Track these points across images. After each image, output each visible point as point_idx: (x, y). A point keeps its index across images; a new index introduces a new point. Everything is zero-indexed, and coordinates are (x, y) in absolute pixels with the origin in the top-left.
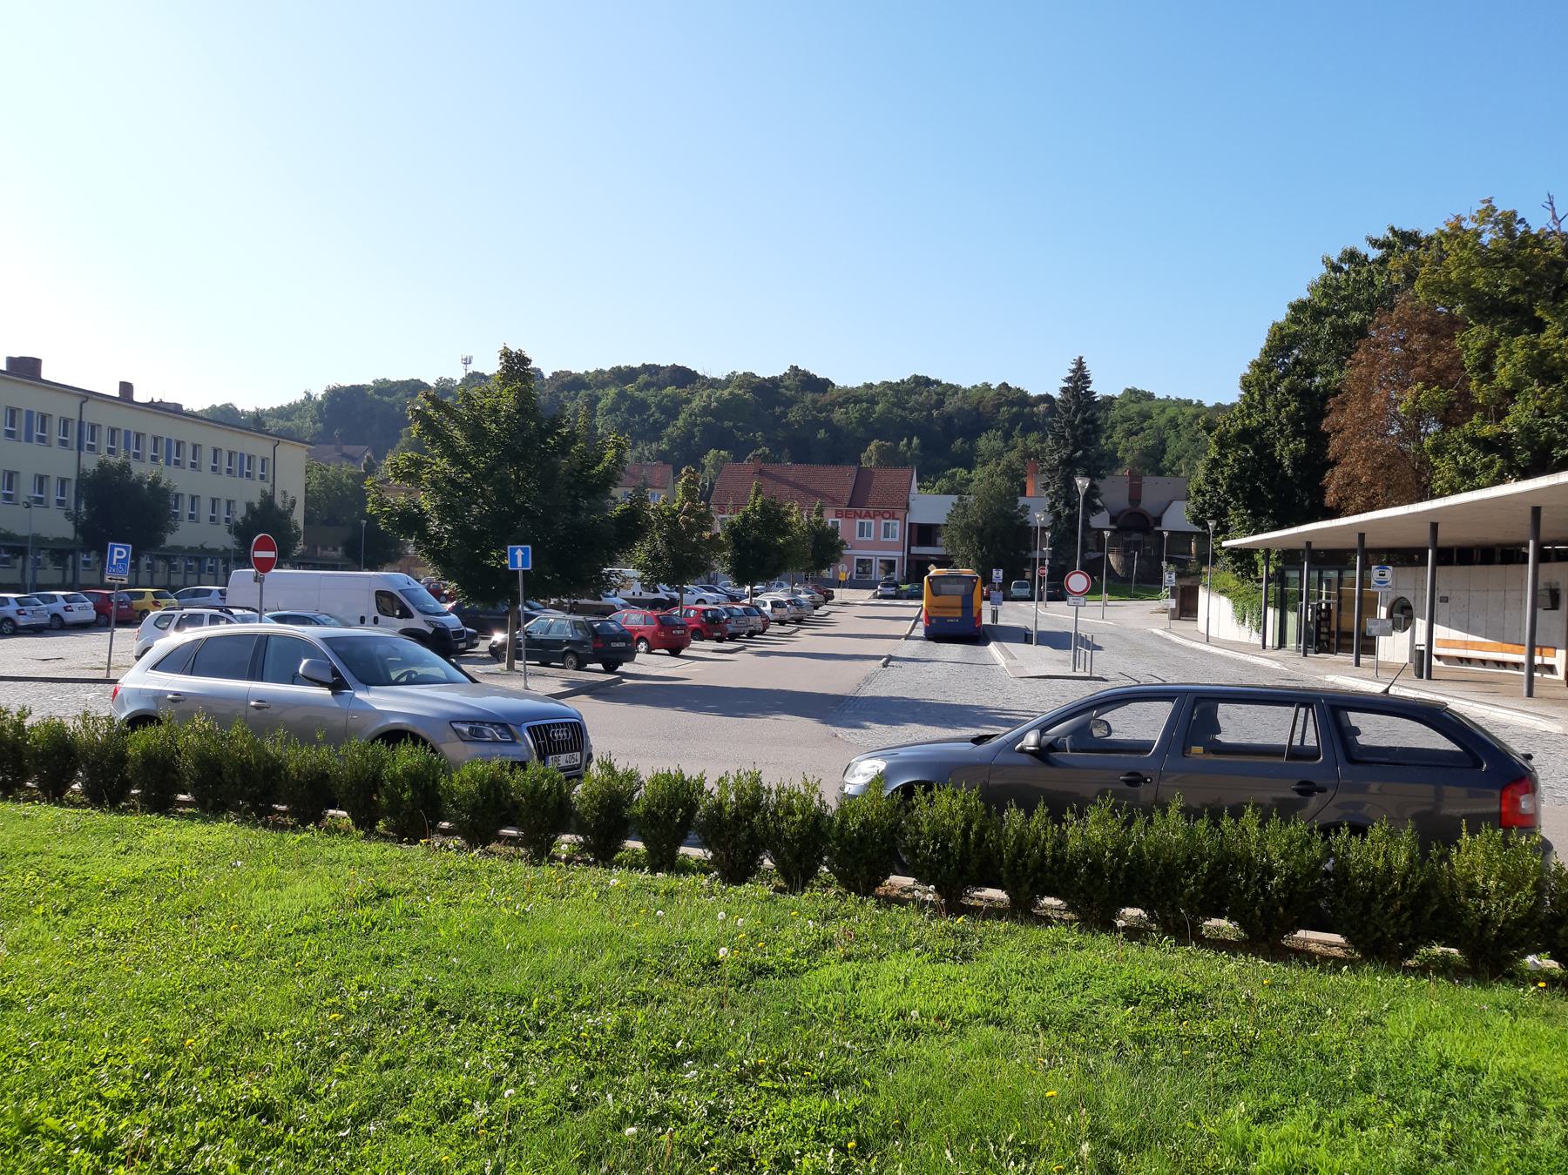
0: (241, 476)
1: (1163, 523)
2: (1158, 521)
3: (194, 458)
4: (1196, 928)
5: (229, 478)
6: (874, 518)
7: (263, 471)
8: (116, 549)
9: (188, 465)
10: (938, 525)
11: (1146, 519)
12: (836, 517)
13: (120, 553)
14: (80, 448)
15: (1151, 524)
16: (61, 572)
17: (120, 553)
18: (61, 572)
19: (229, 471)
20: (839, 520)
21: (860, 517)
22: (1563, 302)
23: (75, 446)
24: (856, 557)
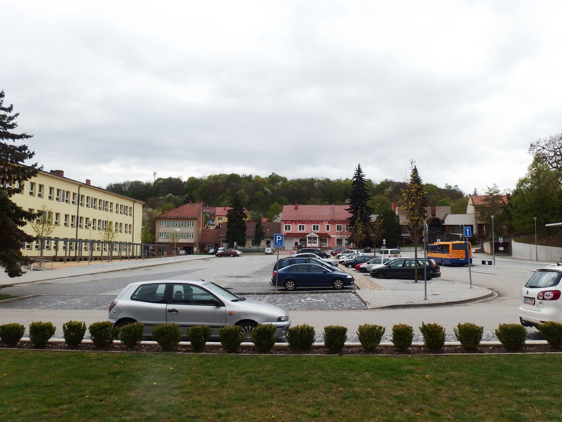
0: (92, 207)
1: (445, 221)
2: (443, 221)
3: (40, 191)
4: (493, 347)
5: (58, 203)
6: (342, 224)
7: (73, 199)
8: (277, 236)
9: (37, 195)
10: (452, 214)
11: (440, 221)
12: (328, 224)
13: (279, 238)
14: (78, 204)
15: (441, 223)
16: (55, 251)
17: (279, 238)
18: (55, 251)
19: (57, 199)
20: (330, 225)
21: (337, 224)
22: (384, 194)
23: (77, 204)
24: (336, 238)
